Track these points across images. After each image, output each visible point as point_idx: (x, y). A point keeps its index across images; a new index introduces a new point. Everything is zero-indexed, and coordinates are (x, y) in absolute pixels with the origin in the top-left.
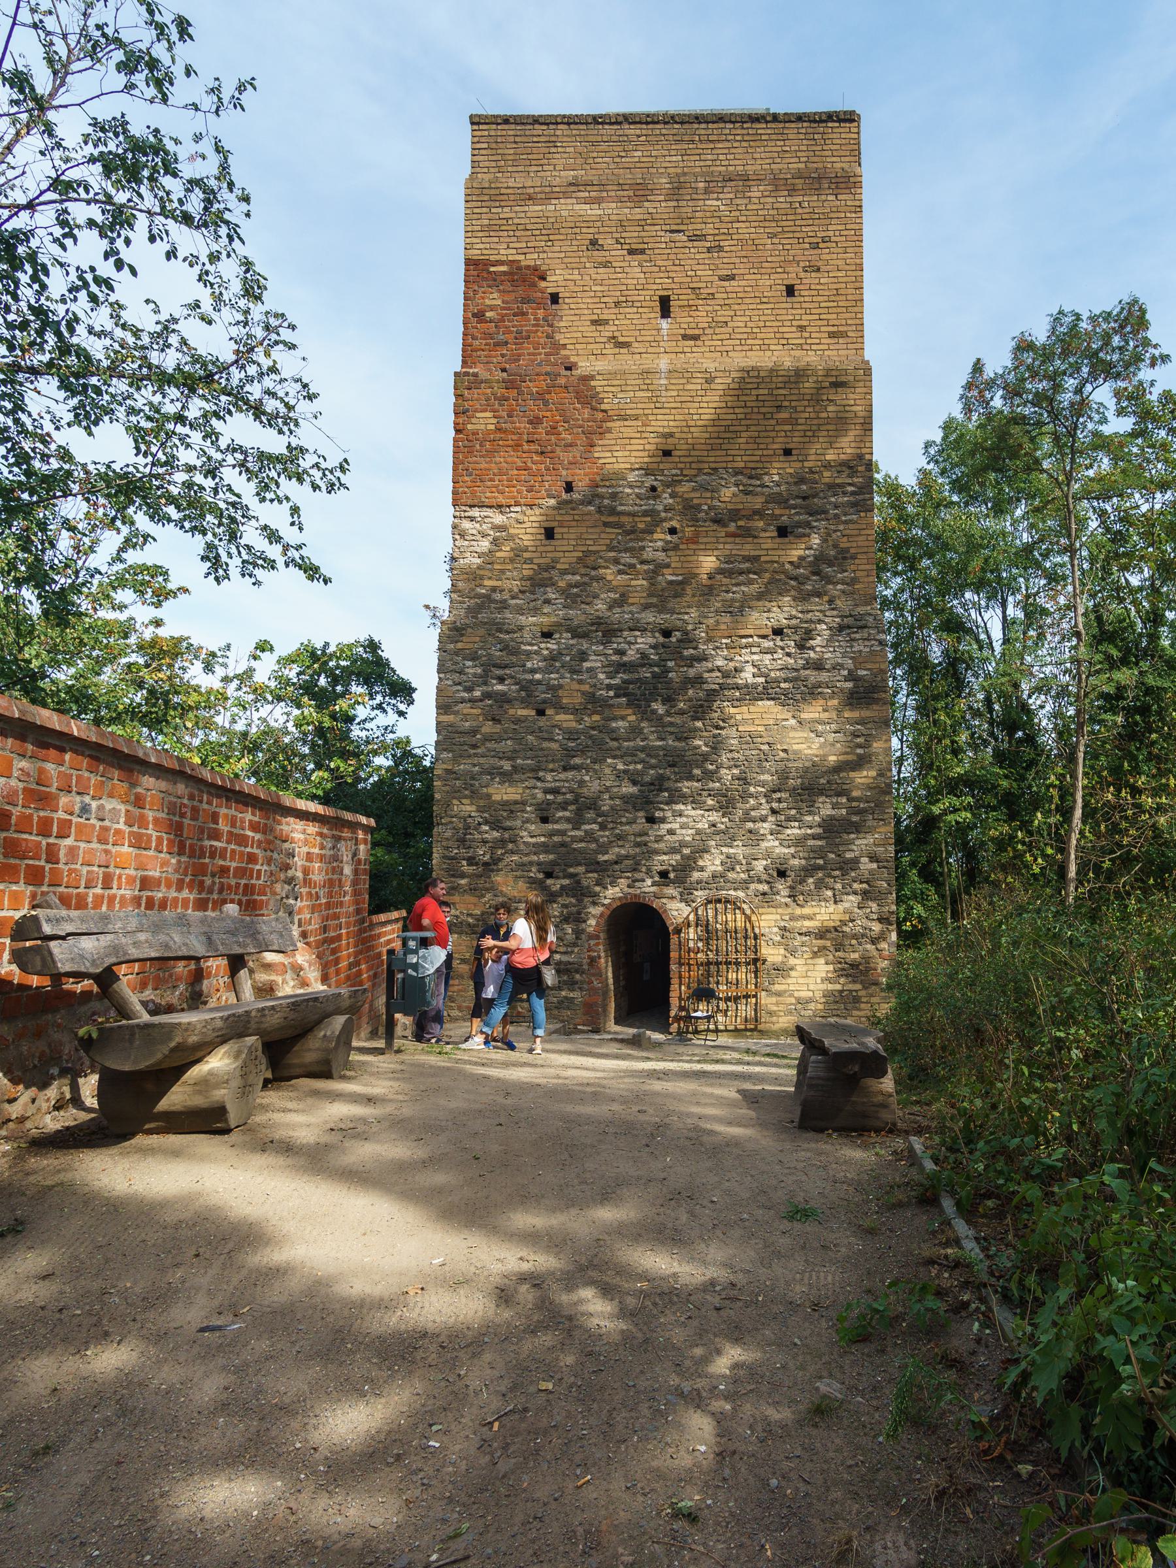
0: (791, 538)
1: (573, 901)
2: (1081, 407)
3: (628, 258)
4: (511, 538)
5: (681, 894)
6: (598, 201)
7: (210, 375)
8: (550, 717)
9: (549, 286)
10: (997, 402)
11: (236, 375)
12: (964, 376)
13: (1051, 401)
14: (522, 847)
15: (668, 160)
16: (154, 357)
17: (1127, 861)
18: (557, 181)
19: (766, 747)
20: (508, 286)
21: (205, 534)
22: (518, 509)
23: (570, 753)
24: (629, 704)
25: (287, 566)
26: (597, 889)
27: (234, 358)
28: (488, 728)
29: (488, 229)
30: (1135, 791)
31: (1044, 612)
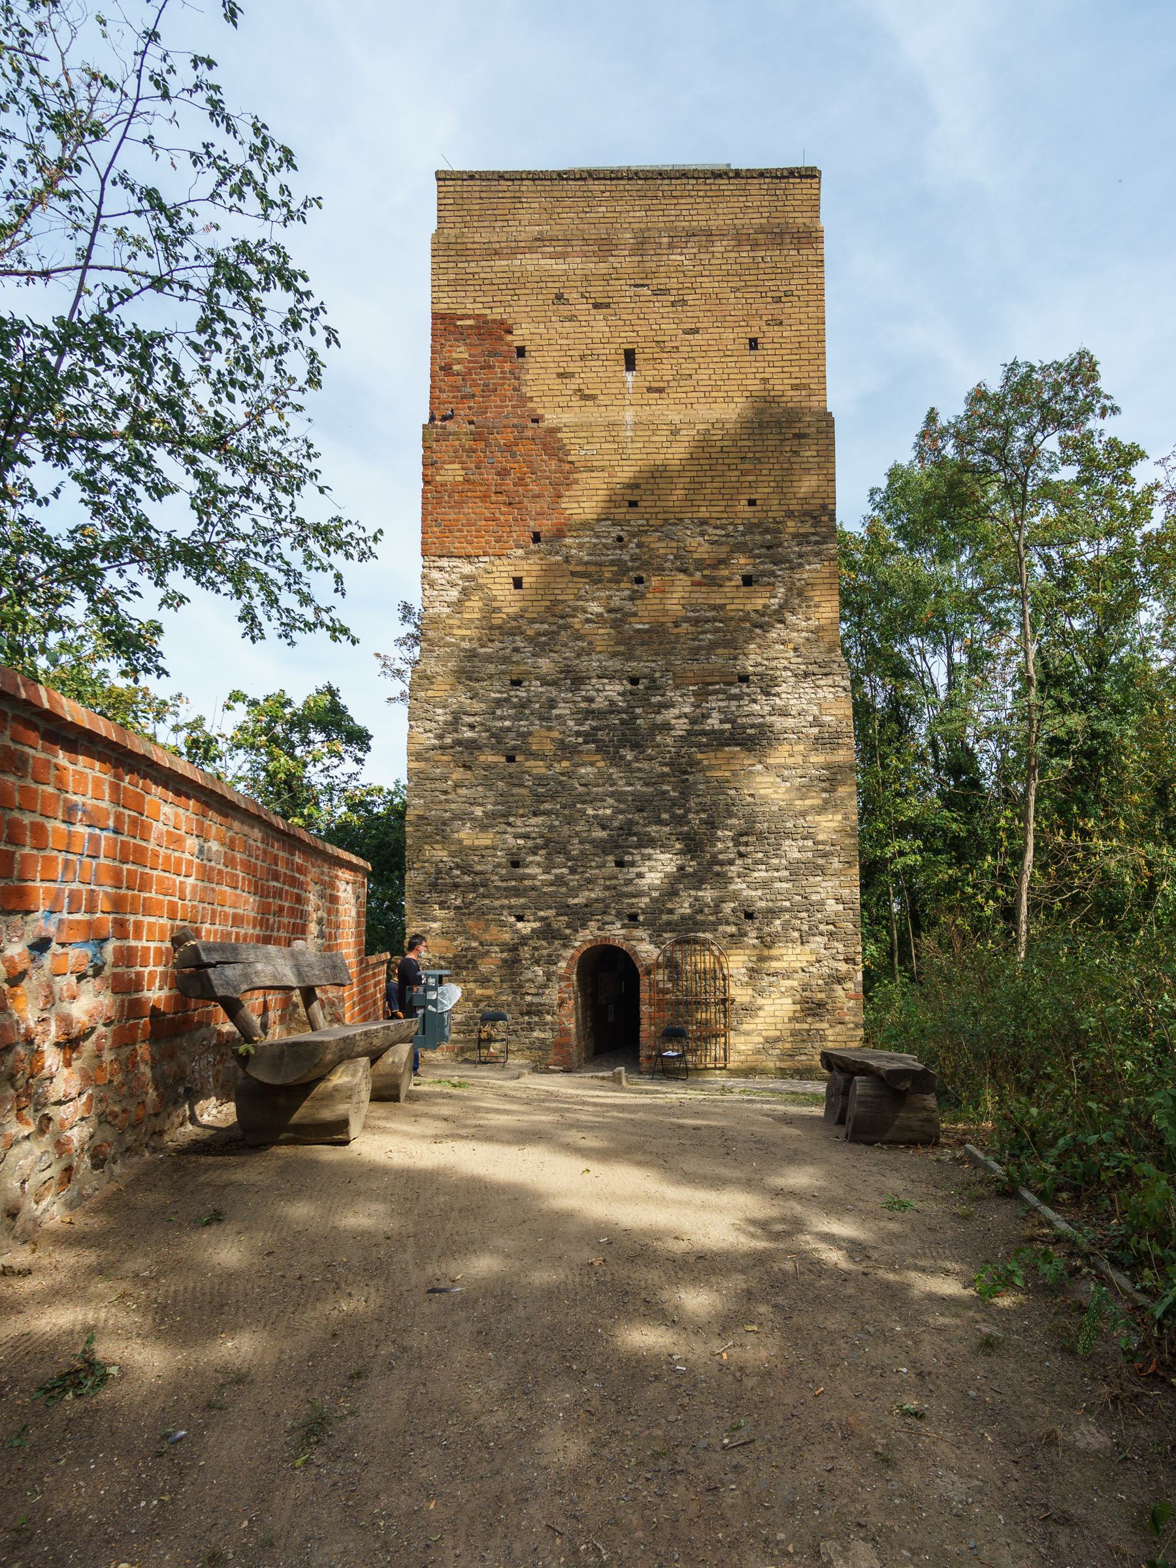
1: (544, 943)
2: (1031, 456)
3: (593, 312)
4: (480, 588)
5: (650, 936)
6: (563, 256)
8: (520, 764)
9: (515, 340)
12: (919, 427)
14: (493, 891)
15: (633, 216)
17: (1076, 901)
18: (523, 236)
20: (475, 340)
23: (539, 799)
24: (598, 750)
26: (568, 931)
28: (458, 774)
29: (455, 284)
30: (1085, 834)
31: (988, 656)
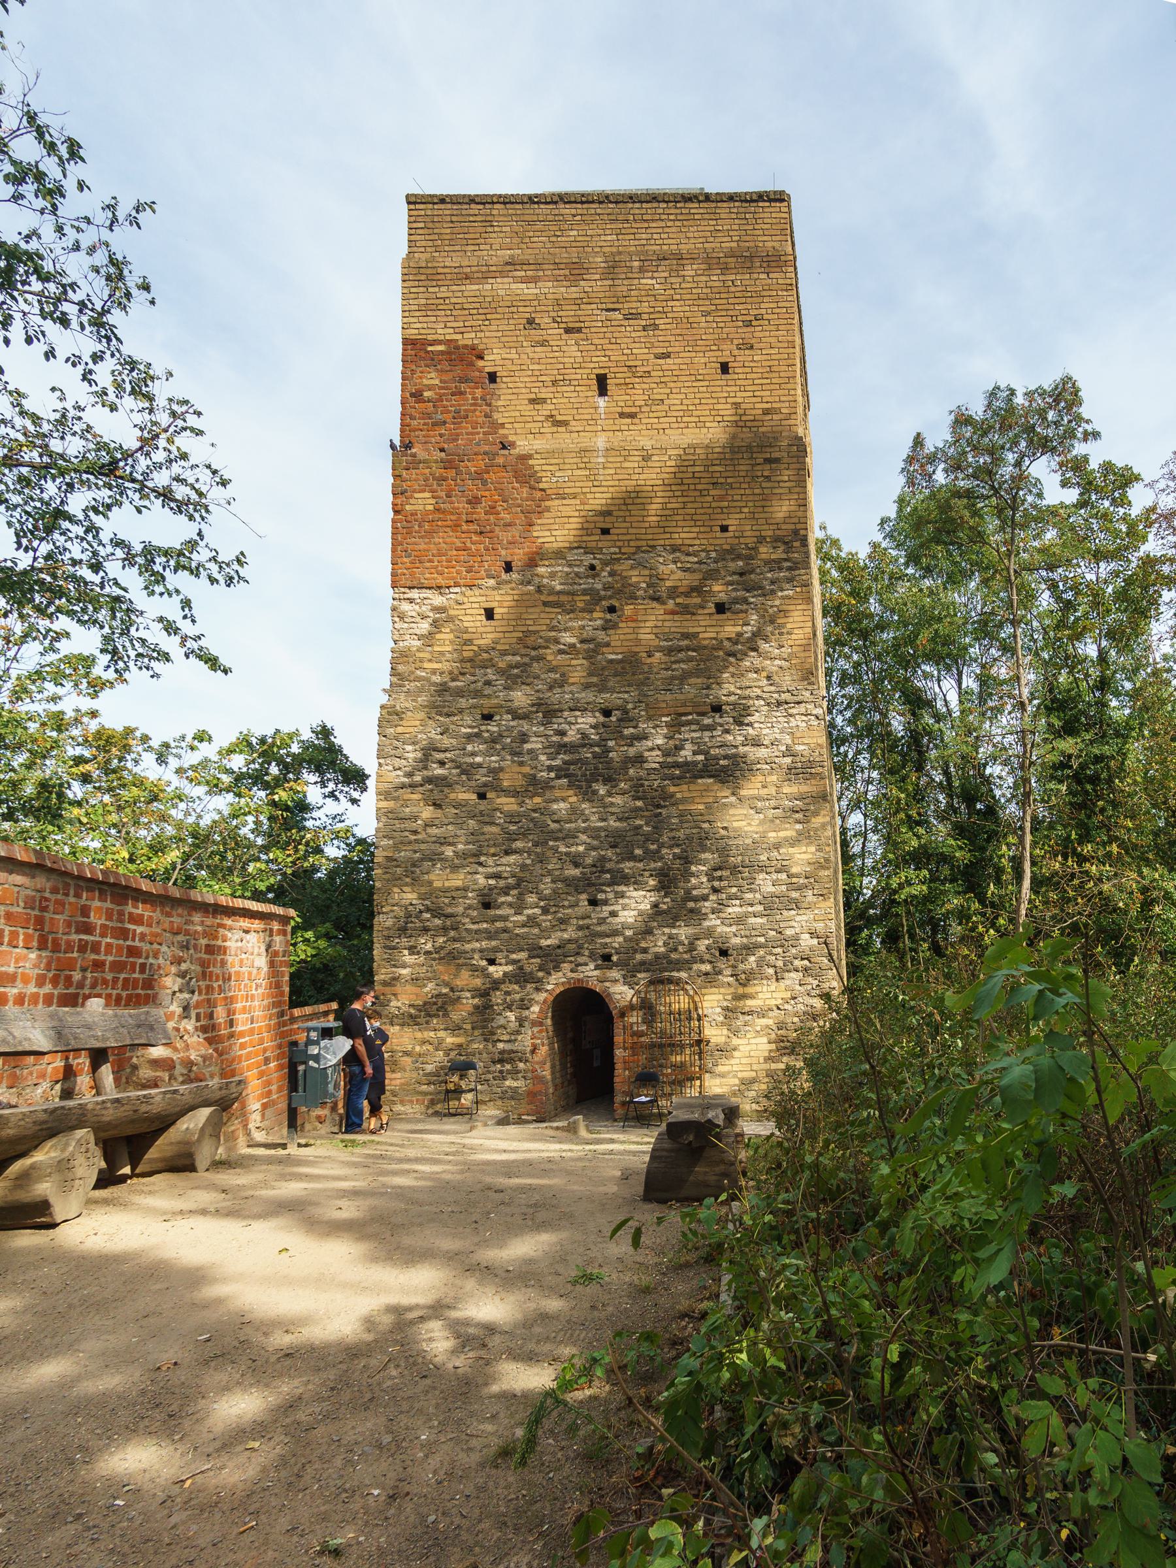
0: (728, 614)
1: (516, 987)
2: (1020, 479)
3: (565, 336)
4: (450, 619)
5: (624, 977)
6: (535, 280)
7: (114, 462)
10: (940, 477)
11: (143, 463)
12: (905, 450)
13: (990, 473)
14: (464, 934)
15: (605, 239)
16: (56, 445)
19: (706, 825)
21: (102, 627)
22: (457, 590)
24: (570, 786)
25: (187, 656)
26: (541, 974)
27: (139, 444)
30: (1082, 859)
